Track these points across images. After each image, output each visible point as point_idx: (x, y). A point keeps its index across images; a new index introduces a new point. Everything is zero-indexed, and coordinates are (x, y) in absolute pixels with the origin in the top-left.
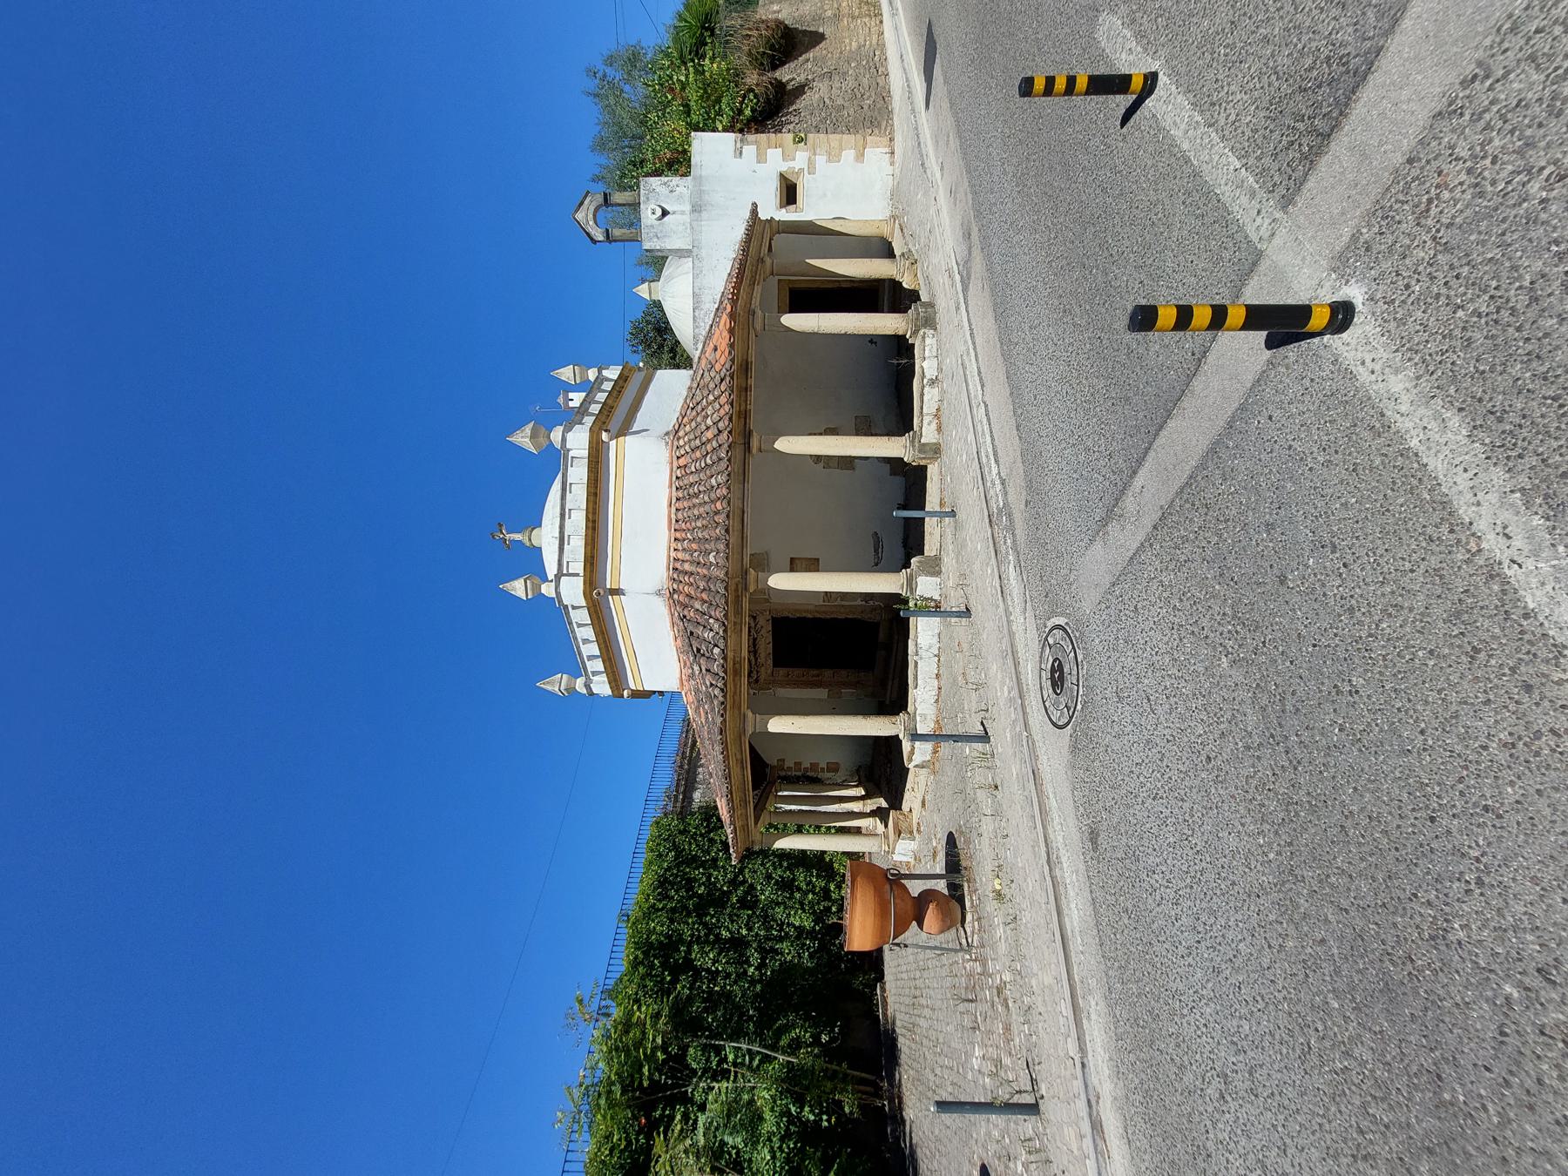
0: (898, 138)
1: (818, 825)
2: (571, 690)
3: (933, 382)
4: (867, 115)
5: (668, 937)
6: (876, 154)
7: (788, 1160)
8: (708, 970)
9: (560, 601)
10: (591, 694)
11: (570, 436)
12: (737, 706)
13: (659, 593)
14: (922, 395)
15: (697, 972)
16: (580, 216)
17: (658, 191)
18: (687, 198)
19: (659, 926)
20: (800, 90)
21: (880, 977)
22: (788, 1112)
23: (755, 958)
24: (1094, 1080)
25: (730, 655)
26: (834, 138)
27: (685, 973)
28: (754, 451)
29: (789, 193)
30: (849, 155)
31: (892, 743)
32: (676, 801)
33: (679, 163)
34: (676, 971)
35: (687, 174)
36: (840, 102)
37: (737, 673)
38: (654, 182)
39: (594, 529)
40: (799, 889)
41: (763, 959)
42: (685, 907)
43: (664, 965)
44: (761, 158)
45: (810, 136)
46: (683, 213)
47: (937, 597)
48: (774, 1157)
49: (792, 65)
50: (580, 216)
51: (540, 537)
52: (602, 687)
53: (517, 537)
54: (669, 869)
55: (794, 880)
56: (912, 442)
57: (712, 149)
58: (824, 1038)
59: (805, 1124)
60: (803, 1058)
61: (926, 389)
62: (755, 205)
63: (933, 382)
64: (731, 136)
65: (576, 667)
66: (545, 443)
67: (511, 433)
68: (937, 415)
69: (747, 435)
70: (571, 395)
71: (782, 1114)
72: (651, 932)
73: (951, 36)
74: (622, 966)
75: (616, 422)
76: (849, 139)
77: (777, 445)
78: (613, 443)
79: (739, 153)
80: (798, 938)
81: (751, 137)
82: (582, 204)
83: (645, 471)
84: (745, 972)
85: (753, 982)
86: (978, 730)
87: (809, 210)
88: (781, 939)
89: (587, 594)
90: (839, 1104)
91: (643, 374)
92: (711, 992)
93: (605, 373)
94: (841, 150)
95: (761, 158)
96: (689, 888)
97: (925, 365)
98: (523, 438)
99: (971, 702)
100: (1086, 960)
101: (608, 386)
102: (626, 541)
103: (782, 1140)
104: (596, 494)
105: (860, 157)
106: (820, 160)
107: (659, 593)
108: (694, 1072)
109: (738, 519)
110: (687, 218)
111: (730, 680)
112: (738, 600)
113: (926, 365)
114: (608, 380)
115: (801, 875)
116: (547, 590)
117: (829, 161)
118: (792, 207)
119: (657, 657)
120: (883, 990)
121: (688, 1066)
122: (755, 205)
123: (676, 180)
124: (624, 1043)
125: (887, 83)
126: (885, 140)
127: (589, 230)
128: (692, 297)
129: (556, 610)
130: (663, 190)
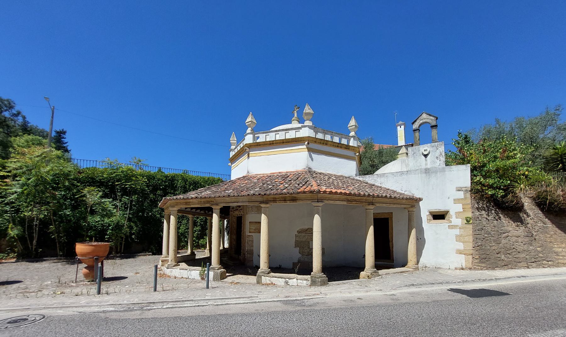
0: (468, 272)
1: (221, 232)
2: (231, 145)
3: (287, 283)
4: (486, 255)
5: (176, 186)
6: (462, 261)
7: (95, 226)
11: (307, 129)
12: (177, 204)
14: (281, 278)
16: (424, 116)
17: (437, 152)
18: (434, 166)
21: (154, 254)
26: (471, 239)
29: (439, 216)
30: (461, 246)
33: (455, 158)
35: (447, 165)
36: (504, 241)
37: (186, 203)
38: (442, 149)
39: (270, 144)
43: (166, 186)
44: (456, 201)
45: (471, 226)
46: (426, 164)
48: (97, 222)
49: (541, 215)
50: (424, 116)
52: (232, 154)
53: (296, 115)
55: (197, 226)
56: (263, 272)
57: (462, 175)
58: (133, 236)
59: (107, 230)
60: (126, 230)
61: (284, 280)
63: (287, 283)
68: (272, 284)
70: (403, 127)
71: (109, 224)
72: (178, 181)
73: (483, 306)
74: (167, 173)
75: (312, 146)
76: (470, 246)
78: (305, 147)
79: (459, 190)
81: (468, 195)
82: (430, 115)
83: (291, 162)
87: (430, 228)
91: (354, 156)
94: (463, 242)
95: (456, 201)
97: (295, 280)
98: (308, 109)
101: (344, 141)
103: (102, 224)
104: (283, 143)
105: (460, 252)
106: (457, 231)
109: (235, 200)
110: (424, 167)
112: (208, 202)
113: (295, 280)
114: (348, 142)
115: (198, 228)
116: (249, 130)
117: (457, 236)
119: (238, 171)
123: (443, 159)
124: (128, 176)
125: (520, 268)
126: (470, 265)
127: (418, 121)
130: (437, 154)
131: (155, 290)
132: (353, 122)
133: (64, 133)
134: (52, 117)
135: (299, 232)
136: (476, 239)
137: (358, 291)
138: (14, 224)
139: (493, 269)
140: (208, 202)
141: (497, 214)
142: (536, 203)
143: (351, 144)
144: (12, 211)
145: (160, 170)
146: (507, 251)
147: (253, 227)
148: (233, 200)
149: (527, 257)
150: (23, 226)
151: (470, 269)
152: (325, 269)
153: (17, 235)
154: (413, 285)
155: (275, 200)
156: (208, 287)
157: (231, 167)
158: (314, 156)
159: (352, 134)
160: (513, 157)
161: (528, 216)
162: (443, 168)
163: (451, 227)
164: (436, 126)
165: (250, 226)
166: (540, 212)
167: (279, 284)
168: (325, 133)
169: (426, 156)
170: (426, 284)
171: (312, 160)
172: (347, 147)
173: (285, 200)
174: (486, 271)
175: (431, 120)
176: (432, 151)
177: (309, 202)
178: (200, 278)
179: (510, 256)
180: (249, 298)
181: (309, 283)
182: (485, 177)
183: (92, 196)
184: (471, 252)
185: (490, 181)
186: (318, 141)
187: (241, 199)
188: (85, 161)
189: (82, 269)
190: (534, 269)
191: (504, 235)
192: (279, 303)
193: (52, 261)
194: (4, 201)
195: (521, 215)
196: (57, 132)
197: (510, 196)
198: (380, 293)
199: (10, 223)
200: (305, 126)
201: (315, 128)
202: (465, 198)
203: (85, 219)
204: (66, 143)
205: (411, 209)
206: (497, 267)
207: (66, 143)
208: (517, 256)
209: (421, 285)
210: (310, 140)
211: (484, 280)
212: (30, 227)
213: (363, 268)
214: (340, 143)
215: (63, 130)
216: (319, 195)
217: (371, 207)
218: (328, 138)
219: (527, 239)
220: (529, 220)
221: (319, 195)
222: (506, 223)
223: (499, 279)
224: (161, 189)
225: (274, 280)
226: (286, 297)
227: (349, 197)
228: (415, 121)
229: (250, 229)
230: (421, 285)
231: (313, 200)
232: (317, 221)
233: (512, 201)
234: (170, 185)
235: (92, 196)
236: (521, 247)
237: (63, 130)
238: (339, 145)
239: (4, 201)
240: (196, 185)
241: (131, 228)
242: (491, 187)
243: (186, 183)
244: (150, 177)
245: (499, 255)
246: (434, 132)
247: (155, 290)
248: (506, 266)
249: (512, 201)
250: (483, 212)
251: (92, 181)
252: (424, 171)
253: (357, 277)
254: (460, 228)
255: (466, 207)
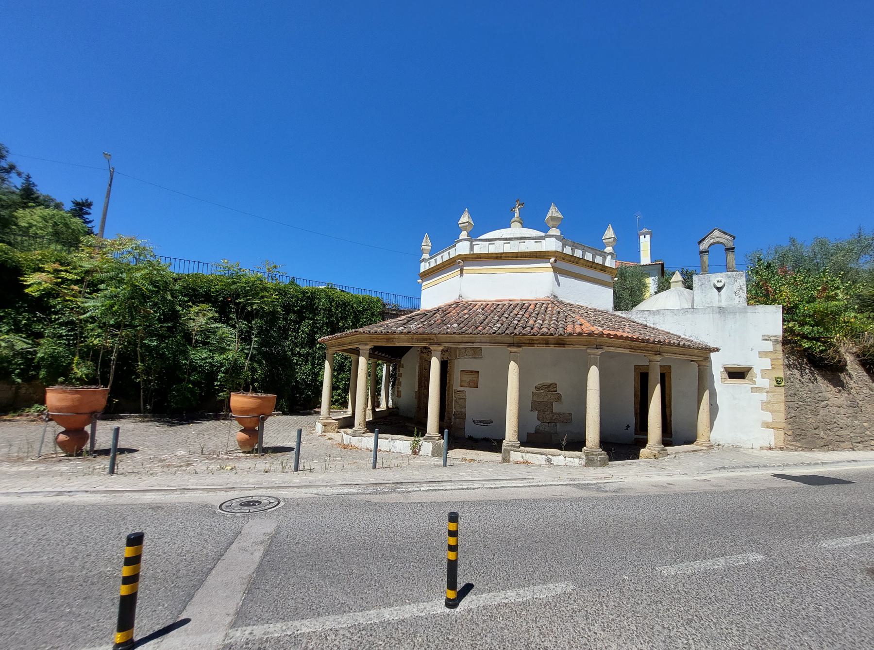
2: (422, 252)
3: (549, 461)
4: (801, 432)
5: (317, 307)
6: (770, 437)
7: (200, 366)
8: (299, 328)
9: (458, 242)
10: (421, 262)
11: (553, 239)
12: (372, 340)
13: (461, 296)
15: (299, 323)
16: (716, 233)
17: (736, 285)
18: (730, 303)
19: (322, 303)
20: (838, 383)
21: (284, 413)
22: (222, 366)
23: (304, 351)
24: (80, 495)
25: (396, 336)
26: (782, 407)
27: (299, 317)
28: (510, 349)
29: (737, 374)
30: (768, 417)
31: (421, 428)
32: (392, 310)
33: (760, 294)
34: (300, 313)
37: (388, 340)
38: (742, 281)
39: (497, 257)
40: (339, 374)
41: (303, 355)
42: (332, 316)
43: (302, 307)
44: (763, 354)
45: (782, 390)
46: (720, 301)
47: (421, 453)
48: (203, 359)
49: (866, 378)
50: (716, 233)
51: (516, 227)
52: (424, 267)
53: (517, 214)
54: (353, 307)
55: (344, 372)
56: (512, 445)
57: (770, 320)
61: (544, 457)
62: (717, 350)
63: (549, 461)
64: (780, 333)
65: (433, 253)
66: (550, 225)
67: (556, 205)
68: (526, 462)
69: (518, 345)
70: (648, 237)
71: (221, 363)
74: (304, 286)
75: (562, 265)
76: (782, 417)
77: (512, 363)
78: (549, 265)
79: (766, 339)
80: (313, 373)
81: (779, 347)
82: (725, 233)
84: (297, 346)
85: (292, 350)
86: (301, 467)
87: (723, 387)
88: (313, 364)
89: (460, 257)
90: (222, 391)
92: (288, 330)
93: (609, 257)
94: (772, 412)
95: (763, 354)
96: (342, 318)
97: (561, 457)
98: (553, 212)
99: (315, 464)
100: (126, 499)
101: (599, 260)
102: (495, 275)
103: (210, 363)
104: (517, 257)
105: (767, 425)
106: (763, 396)
107: (461, 296)
108: (250, 322)
110: (716, 304)
111: (385, 336)
112: (425, 340)
113: (562, 458)
114: (604, 260)
116: (464, 235)
117: (763, 403)
118: (726, 375)
119: (435, 295)
120: (278, 415)
121: (253, 319)
122: (717, 350)
123: (744, 295)
124: (255, 289)
125: (843, 449)
126: (781, 444)
127: (707, 240)
128: (665, 312)
129: (453, 242)
131: (375, 467)
132: (610, 233)
133: (89, 205)
134: (110, 185)
135: (538, 388)
136: (788, 408)
137: (658, 475)
138: (81, 357)
139: (811, 450)
140: (425, 340)
141: (813, 374)
142: (860, 361)
143: (607, 264)
144: (71, 335)
145: (292, 281)
146: (828, 425)
147: (468, 378)
148: (465, 340)
149: (852, 435)
150: (95, 359)
151: (781, 449)
152: (605, 443)
153: (87, 375)
154: (724, 468)
155: (531, 343)
156: (445, 465)
157: (420, 286)
158: (560, 278)
159: (609, 249)
160: (834, 298)
161: (850, 377)
162: (745, 308)
163: (753, 390)
164: (733, 248)
165: (461, 376)
166: (865, 374)
167: (537, 463)
168: (574, 247)
169: (719, 289)
170: (740, 467)
171: (559, 284)
172: (603, 268)
173: (547, 343)
174: (802, 453)
175: (725, 239)
176: (729, 283)
177: (584, 348)
178: (410, 452)
179: (831, 434)
180: (522, 479)
181: (583, 462)
182: (802, 324)
183: (199, 318)
184: (783, 425)
185: (807, 329)
186: (567, 258)
187: (478, 338)
188: (187, 262)
189: (55, 430)
190: (861, 452)
191: (823, 403)
192: (571, 488)
193: (132, 420)
194: (58, 319)
195: (842, 376)
196: (77, 204)
197: (830, 351)
198: (685, 478)
199: (74, 355)
200: (551, 236)
201: (563, 239)
202: (775, 351)
203: (185, 353)
204: (90, 222)
205: (704, 363)
206: (815, 447)
207: (90, 222)
208: (839, 433)
209: (733, 468)
210: (559, 256)
211: (809, 464)
212: (106, 363)
213: (644, 443)
214: (572, 256)
215: (87, 200)
216: (599, 339)
217: (658, 358)
218: (578, 253)
219: (850, 411)
220: (852, 384)
221: (599, 339)
222: (824, 387)
223: (826, 463)
224: (294, 312)
225: (530, 457)
226: (571, 480)
227: (633, 344)
228: (704, 239)
229: (461, 381)
230: (733, 468)
231: (590, 345)
232: (594, 375)
233: (833, 358)
234: (348, 313)
235: (199, 318)
236: (843, 422)
237: (87, 200)
238: (592, 265)
239: (58, 319)
240: (385, 315)
241: (253, 370)
242: (804, 337)
243: (331, 303)
244: (282, 292)
245: (817, 432)
246: (731, 256)
247: (375, 467)
248: (826, 446)
249: (833, 358)
250: (795, 371)
251: (197, 293)
252: (717, 310)
253: (636, 456)
254: (767, 392)
255: (776, 363)
